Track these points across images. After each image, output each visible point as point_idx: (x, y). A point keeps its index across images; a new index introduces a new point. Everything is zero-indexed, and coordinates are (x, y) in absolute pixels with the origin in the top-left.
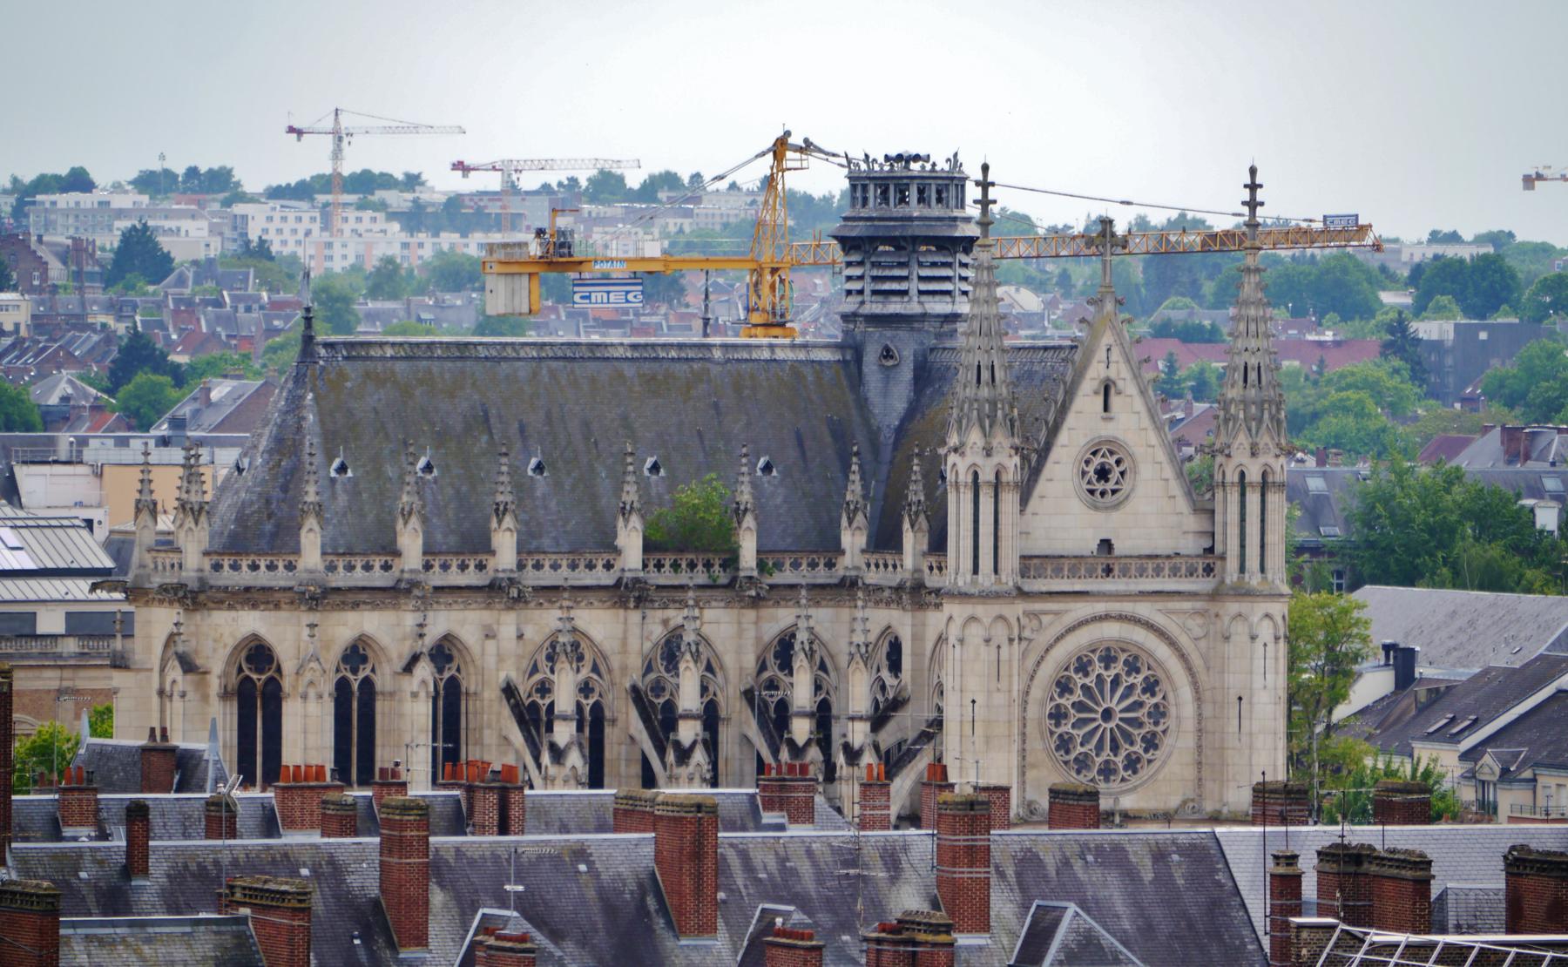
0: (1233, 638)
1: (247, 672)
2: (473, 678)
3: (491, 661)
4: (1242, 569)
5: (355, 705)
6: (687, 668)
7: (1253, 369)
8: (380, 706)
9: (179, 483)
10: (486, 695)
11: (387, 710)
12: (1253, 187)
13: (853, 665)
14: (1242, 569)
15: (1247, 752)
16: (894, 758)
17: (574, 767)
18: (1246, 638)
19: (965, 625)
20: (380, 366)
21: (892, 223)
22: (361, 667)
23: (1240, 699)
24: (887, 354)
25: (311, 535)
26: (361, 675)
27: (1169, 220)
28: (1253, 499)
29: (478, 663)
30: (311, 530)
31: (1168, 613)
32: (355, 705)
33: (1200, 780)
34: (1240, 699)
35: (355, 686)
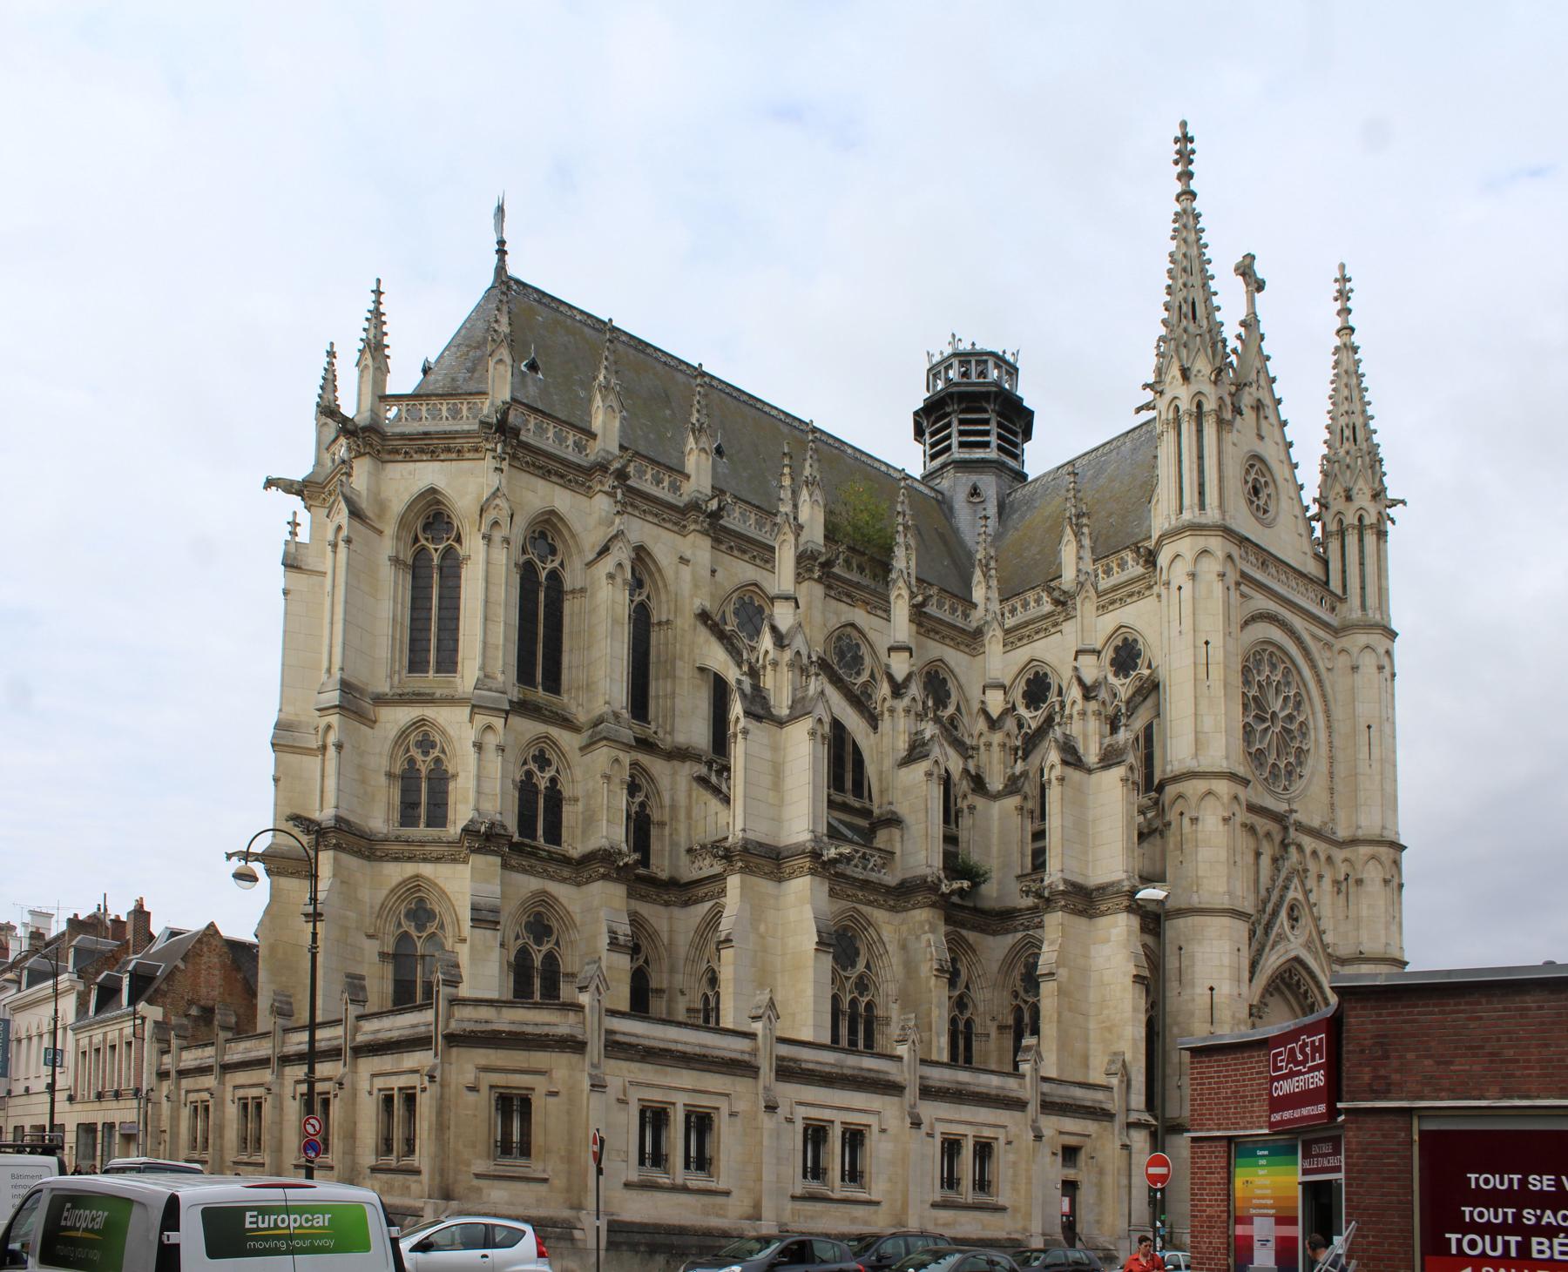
0: (1361, 670)
1: (423, 542)
2: (664, 608)
3: (686, 588)
4: (1363, 606)
5: (542, 596)
6: (899, 595)
7: (1348, 439)
8: (568, 607)
9: (366, 325)
10: (679, 622)
11: (576, 609)
12: (1343, 295)
13: (1083, 594)
14: (1363, 606)
15: (1378, 778)
16: (1069, 759)
17: (798, 653)
18: (1375, 670)
19: (1196, 560)
20: (563, 318)
21: (969, 416)
22: (550, 558)
23: (1369, 727)
24: (975, 492)
25: (501, 367)
26: (549, 566)
27: (893, 821)
28: (1352, 540)
29: (672, 588)
30: (501, 361)
31: (1314, 636)
32: (542, 596)
33: (1332, 805)
34: (1369, 727)
35: (543, 575)
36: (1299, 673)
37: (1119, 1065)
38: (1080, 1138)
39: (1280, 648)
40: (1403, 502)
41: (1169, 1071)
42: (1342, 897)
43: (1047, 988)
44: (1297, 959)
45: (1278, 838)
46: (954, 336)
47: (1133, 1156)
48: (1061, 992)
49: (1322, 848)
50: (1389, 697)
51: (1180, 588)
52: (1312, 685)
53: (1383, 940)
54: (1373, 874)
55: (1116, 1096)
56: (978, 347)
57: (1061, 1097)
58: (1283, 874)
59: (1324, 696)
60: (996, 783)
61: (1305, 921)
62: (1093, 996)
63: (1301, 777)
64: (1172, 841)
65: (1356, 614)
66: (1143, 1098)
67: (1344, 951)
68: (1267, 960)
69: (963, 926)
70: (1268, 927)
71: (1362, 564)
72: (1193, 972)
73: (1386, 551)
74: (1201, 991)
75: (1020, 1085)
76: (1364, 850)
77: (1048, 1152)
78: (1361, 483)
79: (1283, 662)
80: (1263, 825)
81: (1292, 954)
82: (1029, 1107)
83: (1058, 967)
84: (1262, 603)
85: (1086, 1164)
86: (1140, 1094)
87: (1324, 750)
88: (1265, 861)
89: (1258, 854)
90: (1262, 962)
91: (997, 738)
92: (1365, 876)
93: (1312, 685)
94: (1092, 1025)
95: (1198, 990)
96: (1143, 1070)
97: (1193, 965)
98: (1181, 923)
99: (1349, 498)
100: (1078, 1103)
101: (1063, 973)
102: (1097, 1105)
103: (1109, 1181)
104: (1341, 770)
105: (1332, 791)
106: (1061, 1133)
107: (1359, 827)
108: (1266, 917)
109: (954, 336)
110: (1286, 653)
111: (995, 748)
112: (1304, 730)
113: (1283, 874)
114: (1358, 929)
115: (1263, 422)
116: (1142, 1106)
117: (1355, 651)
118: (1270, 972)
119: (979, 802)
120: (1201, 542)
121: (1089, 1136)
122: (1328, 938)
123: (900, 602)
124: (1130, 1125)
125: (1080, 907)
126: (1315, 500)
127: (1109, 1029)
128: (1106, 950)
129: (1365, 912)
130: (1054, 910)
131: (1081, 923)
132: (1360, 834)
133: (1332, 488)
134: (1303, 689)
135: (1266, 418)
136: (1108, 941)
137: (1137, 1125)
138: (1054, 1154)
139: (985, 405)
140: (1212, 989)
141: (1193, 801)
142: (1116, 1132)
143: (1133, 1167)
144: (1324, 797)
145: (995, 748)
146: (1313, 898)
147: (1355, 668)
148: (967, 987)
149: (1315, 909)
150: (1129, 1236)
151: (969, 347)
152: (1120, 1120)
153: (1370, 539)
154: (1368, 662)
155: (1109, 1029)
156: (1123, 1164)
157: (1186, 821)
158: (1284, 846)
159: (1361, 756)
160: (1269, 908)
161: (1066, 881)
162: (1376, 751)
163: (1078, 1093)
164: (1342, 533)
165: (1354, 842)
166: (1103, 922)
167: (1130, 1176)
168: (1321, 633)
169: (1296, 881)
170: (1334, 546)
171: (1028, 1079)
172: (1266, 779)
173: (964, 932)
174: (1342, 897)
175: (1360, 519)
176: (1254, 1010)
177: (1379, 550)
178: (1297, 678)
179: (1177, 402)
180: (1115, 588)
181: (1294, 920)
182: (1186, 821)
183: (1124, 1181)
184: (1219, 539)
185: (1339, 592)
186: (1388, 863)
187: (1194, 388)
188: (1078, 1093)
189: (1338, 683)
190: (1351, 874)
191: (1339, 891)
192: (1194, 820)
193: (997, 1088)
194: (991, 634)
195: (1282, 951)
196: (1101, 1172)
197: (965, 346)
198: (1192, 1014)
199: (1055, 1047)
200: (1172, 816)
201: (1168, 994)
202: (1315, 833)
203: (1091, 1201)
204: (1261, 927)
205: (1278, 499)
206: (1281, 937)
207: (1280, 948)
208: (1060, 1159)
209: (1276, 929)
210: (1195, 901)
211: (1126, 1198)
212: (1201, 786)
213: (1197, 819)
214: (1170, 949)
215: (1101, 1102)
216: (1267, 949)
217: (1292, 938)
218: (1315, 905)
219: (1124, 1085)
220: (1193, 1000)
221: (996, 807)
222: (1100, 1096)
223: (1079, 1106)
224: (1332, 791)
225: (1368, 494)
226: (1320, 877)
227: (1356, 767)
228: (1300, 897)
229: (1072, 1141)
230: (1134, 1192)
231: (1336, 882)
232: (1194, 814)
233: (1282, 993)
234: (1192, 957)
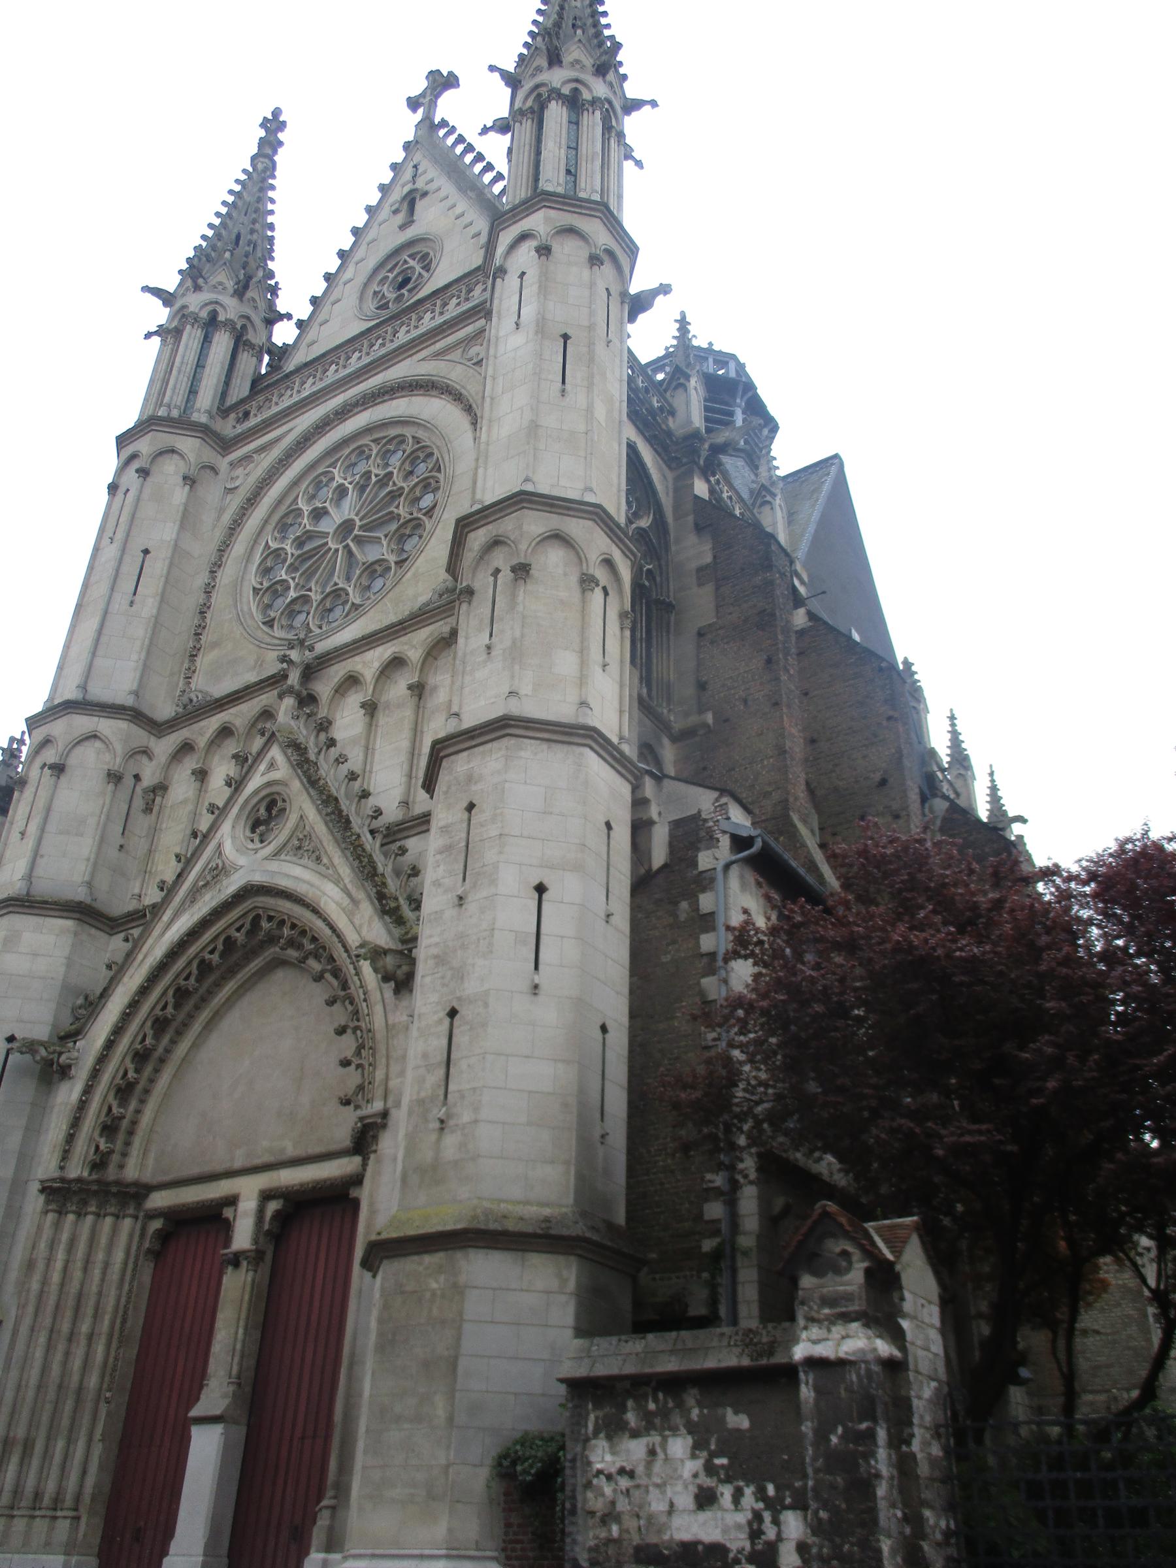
40: (654, 104)
151: (705, 346)
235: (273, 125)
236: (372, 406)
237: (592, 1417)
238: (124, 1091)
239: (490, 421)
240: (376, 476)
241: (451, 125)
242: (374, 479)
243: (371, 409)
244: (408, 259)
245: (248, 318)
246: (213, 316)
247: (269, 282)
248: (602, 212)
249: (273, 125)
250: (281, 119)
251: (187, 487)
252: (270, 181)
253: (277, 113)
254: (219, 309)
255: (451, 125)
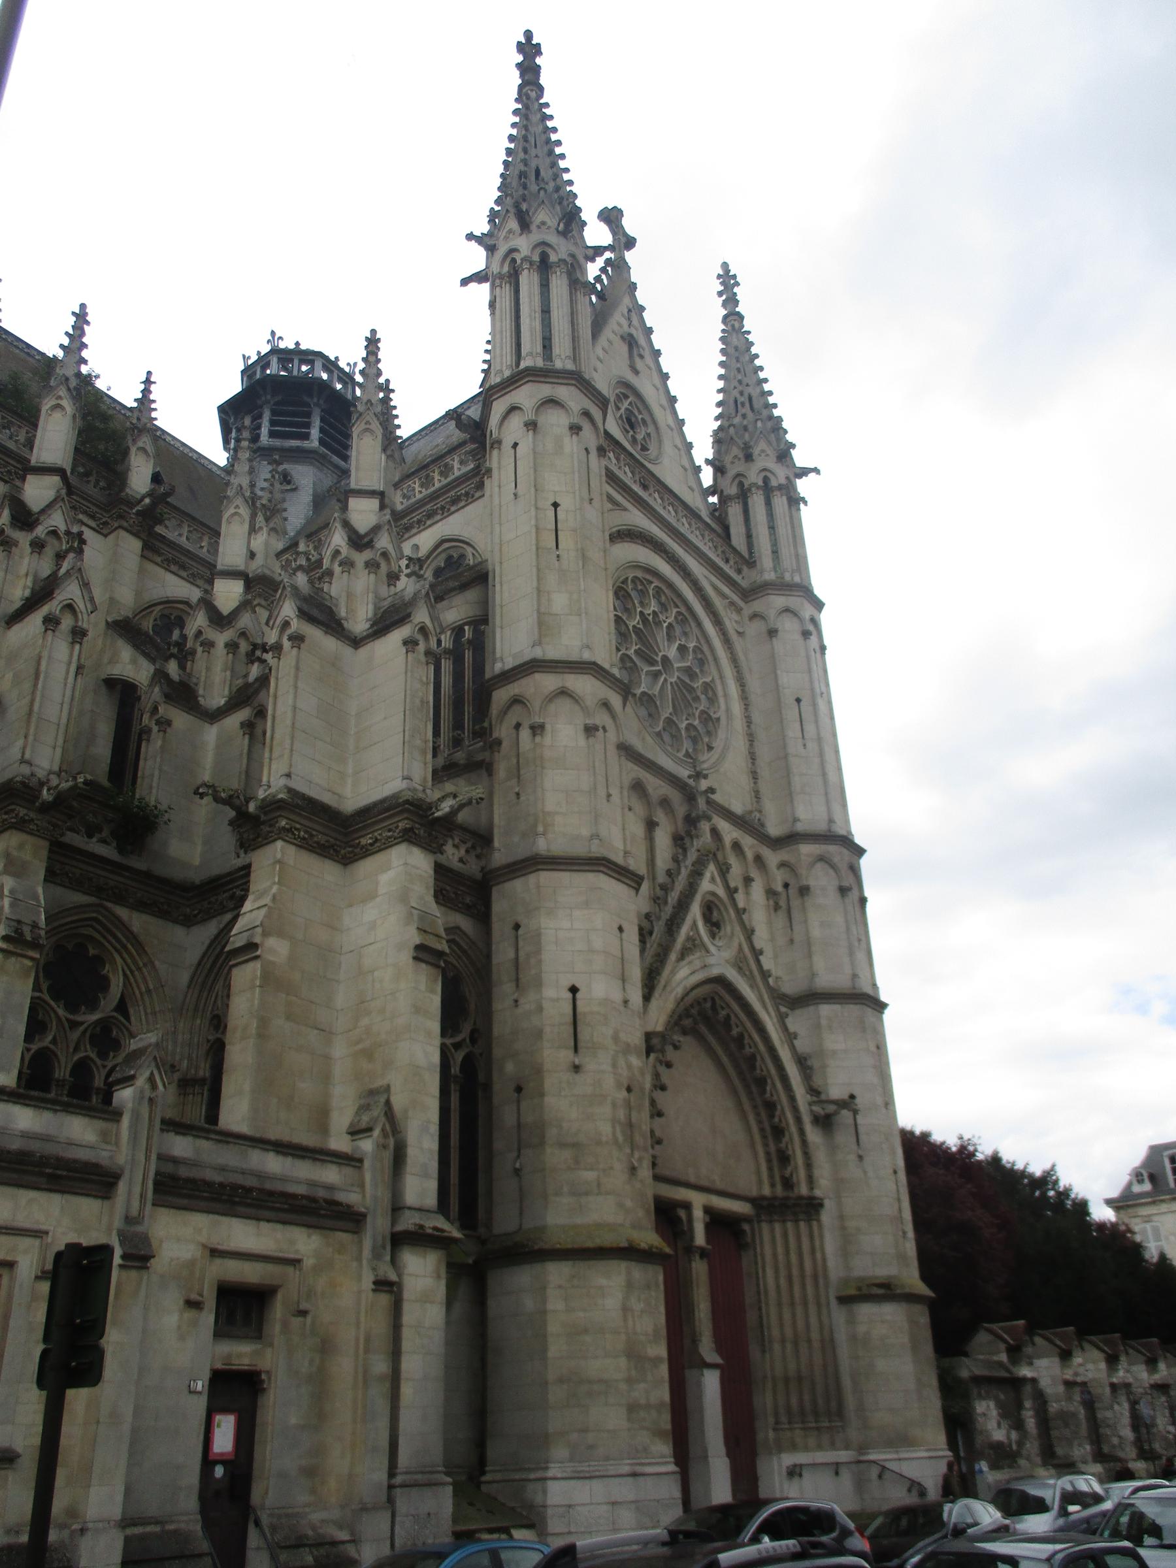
18: (797, 637)
23: (798, 700)
28: (757, 501)
34: (798, 700)
36: (699, 624)
37: (378, 1111)
38: (270, 1267)
39: (671, 586)
40: (816, 471)
41: (498, 1145)
42: (782, 914)
43: (244, 976)
44: (721, 981)
45: (681, 810)
46: (273, 333)
47: (407, 1307)
48: (269, 979)
49: (748, 842)
50: (821, 673)
51: (515, 445)
52: (717, 643)
53: (848, 971)
54: (821, 880)
55: (368, 1177)
56: (303, 347)
57: (223, 1169)
58: (692, 856)
59: (734, 661)
60: (215, 696)
61: (730, 927)
62: (342, 998)
63: (710, 748)
64: (502, 769)
65: (770, 576)
66: (432, 1185)
67: (790, 987)
68: (673, 972)
69: (120, 900)
70: (673, 925)
71: (772, 528)
72: (540, 961)
73: (800, 520)
74: (554, 994)
75: (104, 1136)
76: (807, 850)
77: (172, 1300)
78: (762, 445)
79: (677, 606)
80: (656, 787)
81: (715, 972)
82: (122, 1187)
83: (265, 934)
84: (637, 519)
85: (285, 1325)
86: (426, 1175)
87: (739, 724)
88: (663, 839)
89: (651, 825)
90: (666, 973)
91: (221, 639)
92: (812, 882)
93: (717, 643)
94: (339, 1050)
95: (549, 992)
96: (434, 1128)
97: (538, 951)
98: (518, 886)
99: (749, 458)
100: (268, 1186)
101: (276, 949)
102: (321, 1193)
103: (344, 1366)
104: (764, 753)
105: (754, 775)
106: (215, 1253)
107: (796, 820)
108: (668, 910)
109: (273, 333)
110: (679, 595)
111: (220, 650)
112: (710, 694)
113: (692, 856)
114: (810, 955)
115: (637, 360)
116: (431, 1201)
117: (772, 614)
118: (679, 991)
119: (181, 720)
120: (546, 390)
121: (295, 1262)
122: (767, 962)
123: (57, 415)
124: (399, 1240)
125: (321, 838)
126: (708, 462)
127: (368, 1054)
128: (371, 912)
129: (816, 932)
130: (268, 841)
131: (327, 872)
132: (800, 827)
133: (727, 452)
134: (703, 642)
135: (642, 357)
136: (371, 896)
137: (419, 1239)
138: (193, 1305)
139: (306, 399)
140: (574, 990)
141: (536, 704)
142: (367, 1252)
143: (407, 1333)
144: (745, 781)
145: (220, 650)
146: (740, 898)
147: (772, 633)
148: (122, 1007)
149: (744, 917)
150: (391, 1501)
151: (292, 346)
152: (378, 1225)
153: (780, 502)
154: (788, 626)
155: (368, 1054)
156: (380, 1326)
157: (525, 734)
158: (691, 821)
159: (790, 734)
160: (673, 897)
161: (290, 791)
162: (810, 729)
163: (273, 1164)
164: (744, 495)
165: (791, 839)
166: (366, 866)
167: (395, 1354)
168: (726, 590)
169: (711, 868)
170: (734, 513)
171: (126, 1121)
172: (659, 734)
173: (122, 912)
174: (782, 914)
175: (766, 480)
176: (655, 1041)
177: (791, 517)
178: (696, 630)
179: (516, 255)
180: (434, 497)
181: (714, 926)
182: (525, 734)
183: (381, 1366)
184: (573, 388)
185: (743, 549)
186: (843, 867)
187: (536, 236)
188: (273, 1164)
189: (750, 649)
190: (792, 882)
191: (777, 907)
192: (537, 729)
193: (25, 1135)
194: (232, 510)
195: (697, 964)
196: (326, 1347)
197: (288, 344)
198: (539, 1034)
199: (247, 1087)
200: (503, 731)
201: (497, 1006)
202: (739, 821)
203: (293, 1421)
204: (662, 923)
205: (660, 442)
206: (693, 945)
207: (695, 959)
208: (208, 1318)
209: (684, 931)
210: (542, 846)
211: (382, 1406)
212: (548, 682)
213: (542, 727)
214: (500, 928)
215: (331, 1188)
216: (673, 956)
217: (712, 949)
218: (744, 910)
219: (388, 1155)
220: (540, 1009)
221: (211, 734)
222: (330, 1175)
223: (271, 1193)
224: (754, 775)
225: (773, 455)
226: (748, 880)
227: (785, 747)
228: (721, 892)
229: (250, 1274)
230: (407, 1391)
231: (771, 893)
232: (537, 720)
233: (701, 1039)
234: (537, 936)
235: (529, 49)
236: (441, 520)
237: (26, 561)
238: (771, 1106)
239: (502, 628)
240: (638, 623)
241: (599, 273)
242: (641, 626)
243: (440, 524)
244: (629, 400)
245: (544, 243)
246: (544, 257)
247: (612, 256)
248: (92, 926)
249: (529, 49)
250: (534, 42)
251: (531, 432)
252: (512, 146)
253: (528, 35)
254: (549, 251)
255: (599, 273)
